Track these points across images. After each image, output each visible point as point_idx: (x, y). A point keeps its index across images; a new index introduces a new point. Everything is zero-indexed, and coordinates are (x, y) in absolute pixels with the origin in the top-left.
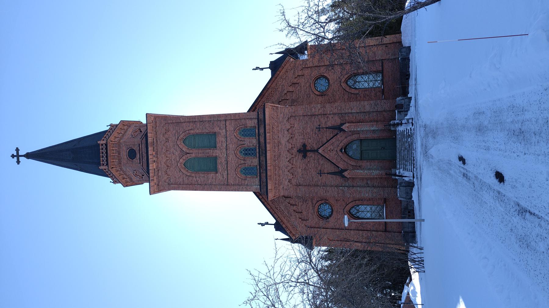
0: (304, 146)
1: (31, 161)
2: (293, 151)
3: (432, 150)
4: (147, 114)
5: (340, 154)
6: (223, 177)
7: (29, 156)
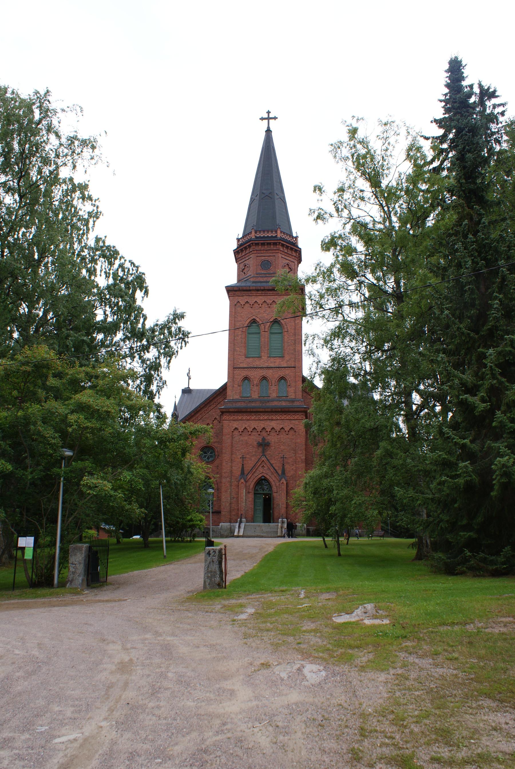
6: (241, 363)
7: (268, 131)
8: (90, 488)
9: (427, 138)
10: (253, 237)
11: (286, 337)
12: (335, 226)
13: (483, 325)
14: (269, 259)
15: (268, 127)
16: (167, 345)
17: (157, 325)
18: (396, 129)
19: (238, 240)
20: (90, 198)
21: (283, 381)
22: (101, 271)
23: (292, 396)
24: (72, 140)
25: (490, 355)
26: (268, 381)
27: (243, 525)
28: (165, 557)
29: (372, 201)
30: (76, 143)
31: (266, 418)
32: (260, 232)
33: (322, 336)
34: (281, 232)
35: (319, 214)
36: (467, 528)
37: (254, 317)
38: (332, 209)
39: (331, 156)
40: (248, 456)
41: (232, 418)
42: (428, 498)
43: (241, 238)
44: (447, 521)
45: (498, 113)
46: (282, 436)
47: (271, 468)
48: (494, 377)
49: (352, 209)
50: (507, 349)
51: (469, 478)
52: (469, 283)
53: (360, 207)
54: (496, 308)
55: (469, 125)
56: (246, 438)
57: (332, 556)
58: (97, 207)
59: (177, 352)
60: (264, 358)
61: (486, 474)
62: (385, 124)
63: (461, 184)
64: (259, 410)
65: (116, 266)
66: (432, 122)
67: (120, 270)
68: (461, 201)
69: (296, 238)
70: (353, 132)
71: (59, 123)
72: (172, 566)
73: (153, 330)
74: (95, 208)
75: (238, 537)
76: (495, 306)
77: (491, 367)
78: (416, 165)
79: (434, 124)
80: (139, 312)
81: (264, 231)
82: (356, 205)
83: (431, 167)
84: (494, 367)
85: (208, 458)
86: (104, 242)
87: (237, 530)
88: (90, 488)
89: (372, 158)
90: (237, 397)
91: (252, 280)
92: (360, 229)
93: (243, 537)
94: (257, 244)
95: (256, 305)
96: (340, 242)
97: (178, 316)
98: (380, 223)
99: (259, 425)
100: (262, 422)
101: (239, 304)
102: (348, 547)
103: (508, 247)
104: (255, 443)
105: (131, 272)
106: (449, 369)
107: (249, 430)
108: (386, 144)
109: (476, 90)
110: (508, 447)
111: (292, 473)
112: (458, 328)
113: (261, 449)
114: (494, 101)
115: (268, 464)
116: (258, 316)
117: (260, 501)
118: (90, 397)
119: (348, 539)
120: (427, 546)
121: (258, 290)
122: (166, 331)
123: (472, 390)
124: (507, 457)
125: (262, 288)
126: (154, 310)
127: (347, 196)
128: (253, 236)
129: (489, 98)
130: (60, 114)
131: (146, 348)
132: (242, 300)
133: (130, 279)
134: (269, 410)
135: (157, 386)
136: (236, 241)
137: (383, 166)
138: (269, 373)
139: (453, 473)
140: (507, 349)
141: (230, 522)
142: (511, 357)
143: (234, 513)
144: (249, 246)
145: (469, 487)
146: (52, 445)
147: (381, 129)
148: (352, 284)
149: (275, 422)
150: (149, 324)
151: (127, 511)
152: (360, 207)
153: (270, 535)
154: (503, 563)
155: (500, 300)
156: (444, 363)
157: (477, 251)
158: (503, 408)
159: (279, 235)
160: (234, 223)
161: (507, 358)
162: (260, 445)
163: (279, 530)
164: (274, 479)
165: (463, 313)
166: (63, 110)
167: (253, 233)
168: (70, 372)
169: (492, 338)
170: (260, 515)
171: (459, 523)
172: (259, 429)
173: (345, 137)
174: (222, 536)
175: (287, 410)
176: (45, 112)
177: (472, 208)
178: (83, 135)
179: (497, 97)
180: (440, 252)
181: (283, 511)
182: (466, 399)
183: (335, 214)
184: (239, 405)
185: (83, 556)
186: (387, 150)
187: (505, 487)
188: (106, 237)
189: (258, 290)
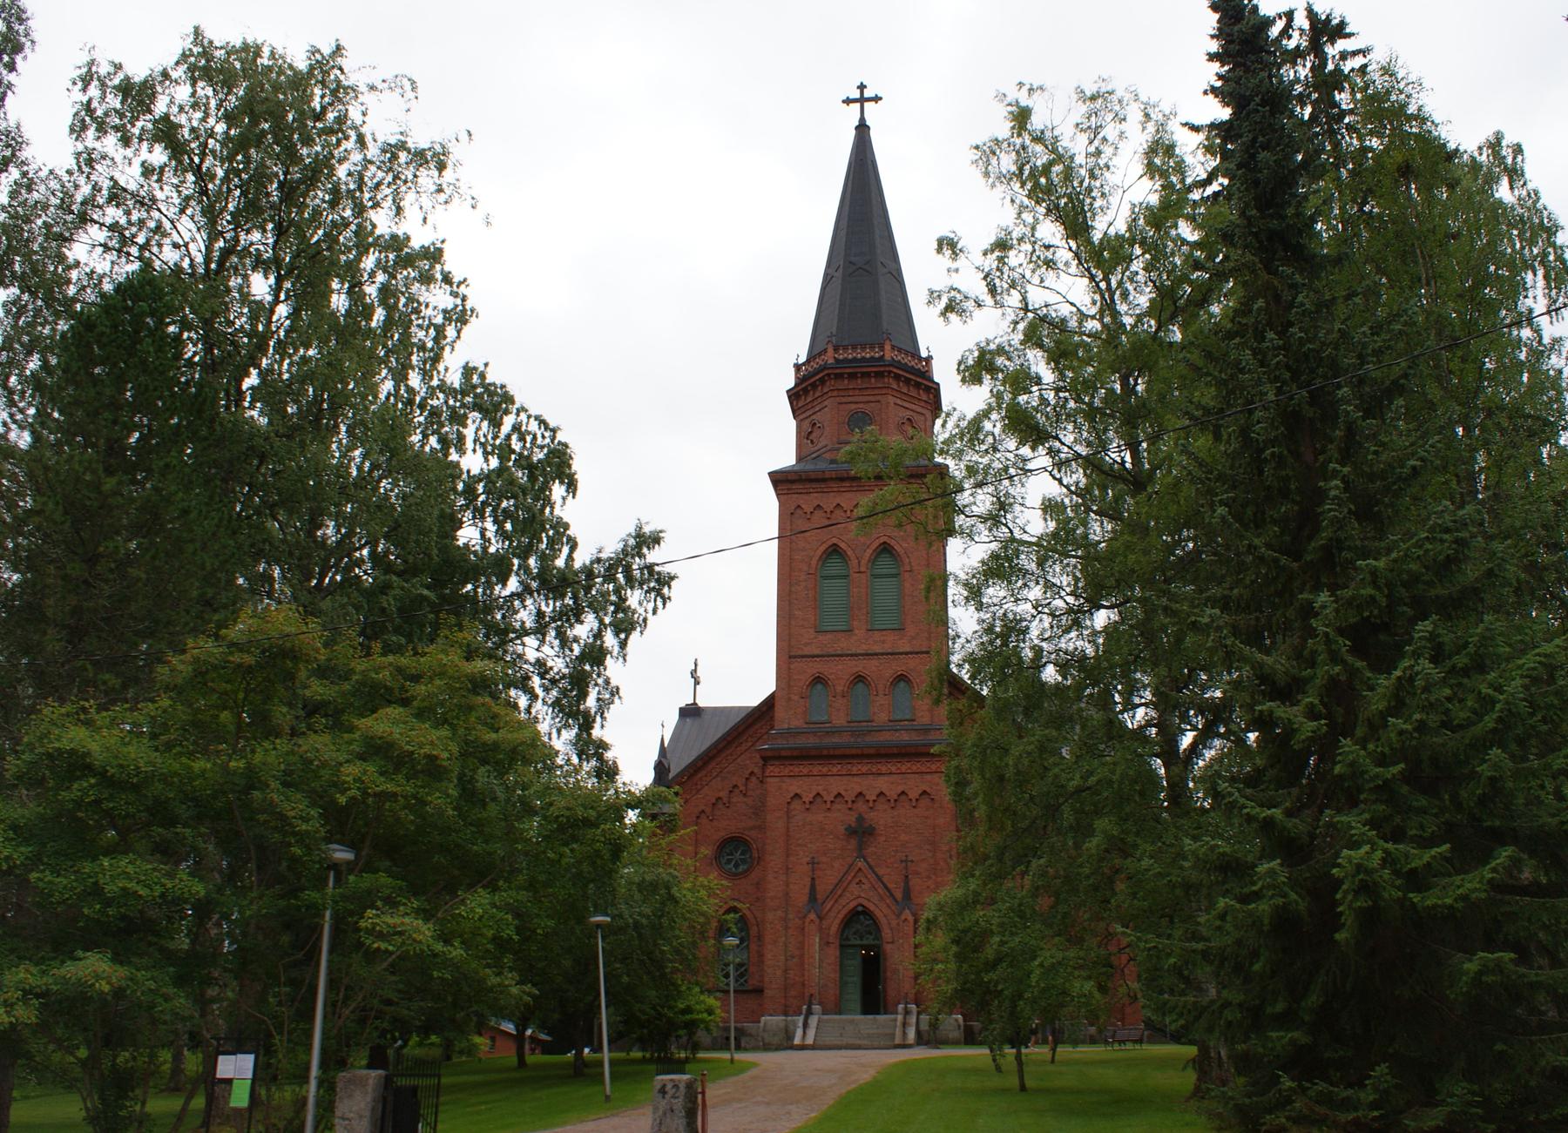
1: (850, 135)
6: (806, 644)
7: (862, 129)
8: (381, 936)
9: (1195, 129)
10: (831, 361)
11: (907, 585)
12: (992, 325)
13: (1310, 538)
14: (867, 408)
15: (862, 119)
16: (621, 606)
17: (599, 560)
18: (1117, 108)
19: (798, 367)
20: (447, 279)
21: (902, 684)
22: (475, 441)
24: (391, 151)
25: (1324, 607)
26: (868, 685)
27: (813, 1021)
28: (607, 1098)
29: (1073, 269)
30: (403, 157)
31: (865, 769)
32: (845, 348)
33: (963, 576)
34: (893, 347)
35: (951, 300)
36: (1286, 1020)
37: (835, 540)
38: (979, 289)
39: (976, 173)
40: (824, 859)
41: (786, 772)
42: (1194, 951)
44: (1240, 1005)
45: (1352, 70)
48: (1334, 658)
49: (1029, 287)
50: (1363, 592)
51: (1280, 901)
52: (1273, 442)
53: (1046, 284)
54: (1336, 497)
55: (1263, 90)
57: (1005, 1091)
58: (464, 299)
59: (645, 620)
61: (1323, 890)
62: (1093, 98)
63: (1249, 219)
64: (848, 752)
65: (506, 428)
66: (1205, 93)
67: (514, 437)
68: (1249, 257)
69: (929, 359)
70: (1021, 117)
71: (364, 114)
72: (616, 1121)
73: (589, 572)
74: (459, 301)
75: (803, 1047)
76: (1333, 493)
77: (1326, 634)
78: (1167, 187)
79: (1211, 96)
80: (557, 532)
81: (854, 347)
82: (1036, 280)
83: (1209, 191)
84: (1332, 634)
85: (736, 866)
86: (482, 376)
87: (799, 1032)
88: (381, 936)
89: (1068, 174)
90: (797, 723)
91: (827, 456)
92: (1042, 329)
93: (813, 1047)
94: (839, 376)
96: (1000, 361)
97: (645, 540)
98: (1093, 317)
100: (856, 779)
102: (1052, 1068)
103: (1360, 356)
104: (842, 829)
105: (539, 441)
106: (1229, 642)
108: (1096, 143)
109: (1301, 20)
110: (1373, 823)
112: (1250, 546)
113: (854, 842)
114: (1342, 45)
117: (855, 964)
118: (395, 722)
119: (1054, 1050)
120: (1220, 1065)
121: (842, 479)
122: (620, 576)
123: (1286, 692)
124: (1367, 848)
126: (592, 523)
127: (1015, 258)
128: (829, 358)
129: (1332, 42)
130: (367, 98)
131: (577, 615)
133: (539, 455)
134: (872, 751)
135: (599, 700)
136: (792, 371)
137: (1090, 190)
138: (870, 667)
139: (1246, 890)
140: (1363, 592)
141: (786, 1015)
142: (1376, 612)
143: (793, 993)
144: (822, 381)
145: (1284, 922)
146: (301, 837)
147: (1084, 108)
148: (1041, 460)
149: (886, 778)
150: (582, 558)
151: (491, 990)
152: (1046, 284)
153: (876, 1044)
154: (1374, 1106)
155: (1344, 480)
156: (1219, 629)
157: (1288, 367)
158: (1360, 732)
159: (889, 354)
160: (787, 327)
161: (1366, 614)
162: (852, 832)
163: (898, 1032)
164: (886, 911)
165: (1264, 513)
166: (372, 88)
168: (359, 668)
169: (1330, 567)
170: (854, 995)
171: (1269, 1010)
172: (850, 796)
173: (1004, 129)
174: (767, 1047)
176: (339, 92)
177: (1275, 273)
178: (418, 141)
179: (1349, 35)
180: (1208, 374)
182: (1271, 713)
183: (989, 301)
185: (369, 1098)
186: (1098, 153)
187: (1370, 919)
188: (486, 365)
189: (842, 479)
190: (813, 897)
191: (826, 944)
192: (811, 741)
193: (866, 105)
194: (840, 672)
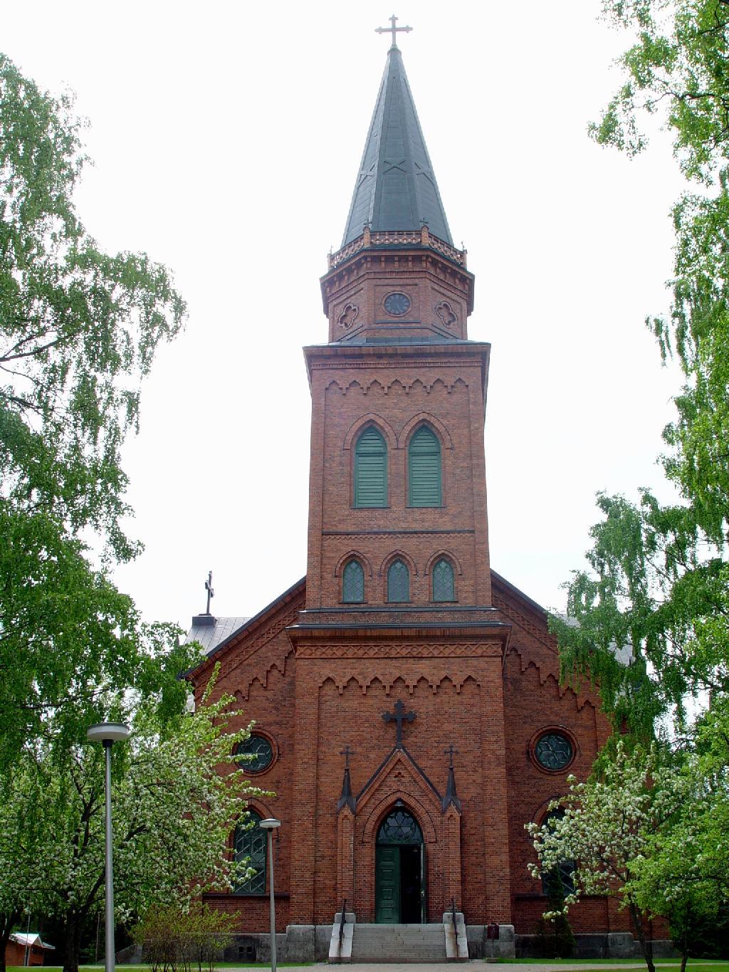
0: (397, 19)
1: (383, 61)
2: (399, 690)
3: (301, 662)
4: (488, 345)
5: (393, 798)
6: (340, 521)
7: (394, 52)
19: (332, 258)
23: (468, 600)
27: (349, 929)
31: (404, 652)
37: (371, 416)
40: (359, 750)
43: (338, 253)
46: (445, 698)
47: (420, 778)
56: (355, 704)
60: (398, 510)
69: (463, 254)
75: (339, 960)
90: (331, 603)
93: (352, 960)
95: (376, 389)
99: (388, 671)
101: (335, 387)
104: (379, 716)
107: (361, 682)
111: (473, 791)
113: (392, 732)
115: (411, 767)
116: (382, 414)
117: (393, 864)
121: (380, 356)
125: (390, 351)
132: (344, 377)
134: (413, 633)
138: (409, 546)
141: (315, 922)
159: (426, 242)
162: (390, 720)
167: (367, 236)
170: (390, 903)
172: (387, 681)
175: (457, 633)
181: (454, 890)
184: (334, 622)
189: (380, 356)
190: (347, 791)
191: (360, 843)
192: (346, 622)
193: (397, 33)
194: (377, 551)
